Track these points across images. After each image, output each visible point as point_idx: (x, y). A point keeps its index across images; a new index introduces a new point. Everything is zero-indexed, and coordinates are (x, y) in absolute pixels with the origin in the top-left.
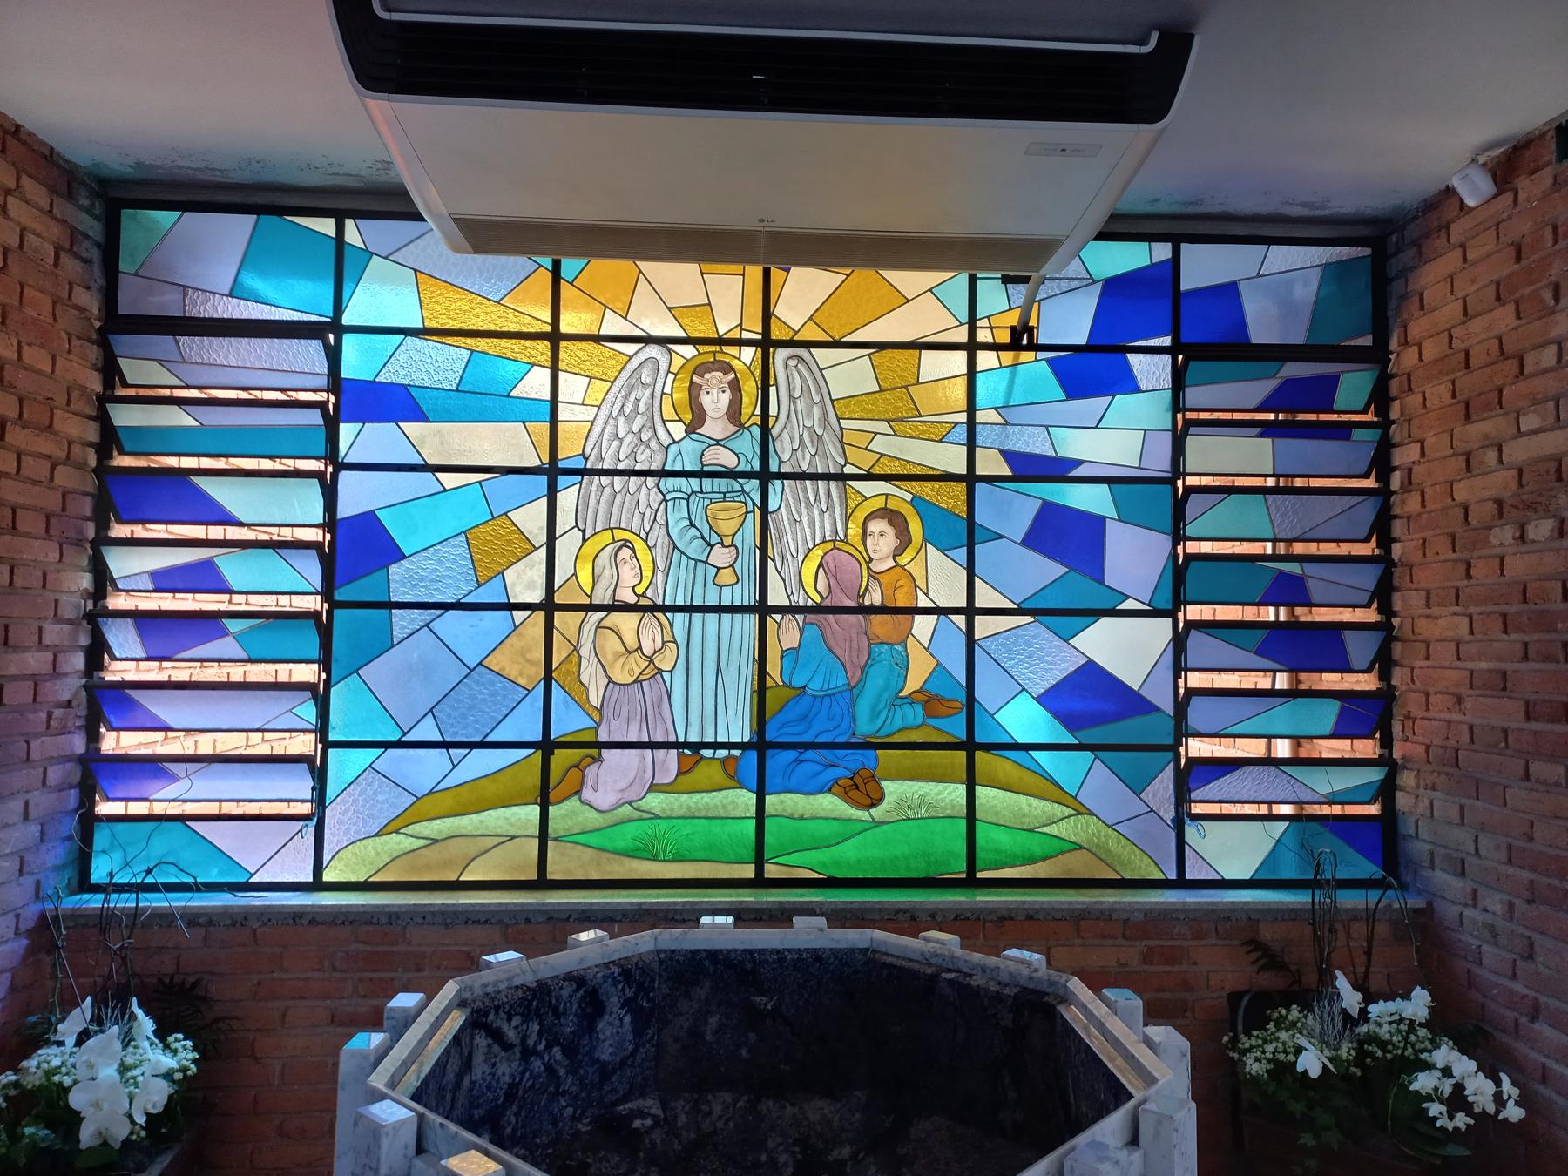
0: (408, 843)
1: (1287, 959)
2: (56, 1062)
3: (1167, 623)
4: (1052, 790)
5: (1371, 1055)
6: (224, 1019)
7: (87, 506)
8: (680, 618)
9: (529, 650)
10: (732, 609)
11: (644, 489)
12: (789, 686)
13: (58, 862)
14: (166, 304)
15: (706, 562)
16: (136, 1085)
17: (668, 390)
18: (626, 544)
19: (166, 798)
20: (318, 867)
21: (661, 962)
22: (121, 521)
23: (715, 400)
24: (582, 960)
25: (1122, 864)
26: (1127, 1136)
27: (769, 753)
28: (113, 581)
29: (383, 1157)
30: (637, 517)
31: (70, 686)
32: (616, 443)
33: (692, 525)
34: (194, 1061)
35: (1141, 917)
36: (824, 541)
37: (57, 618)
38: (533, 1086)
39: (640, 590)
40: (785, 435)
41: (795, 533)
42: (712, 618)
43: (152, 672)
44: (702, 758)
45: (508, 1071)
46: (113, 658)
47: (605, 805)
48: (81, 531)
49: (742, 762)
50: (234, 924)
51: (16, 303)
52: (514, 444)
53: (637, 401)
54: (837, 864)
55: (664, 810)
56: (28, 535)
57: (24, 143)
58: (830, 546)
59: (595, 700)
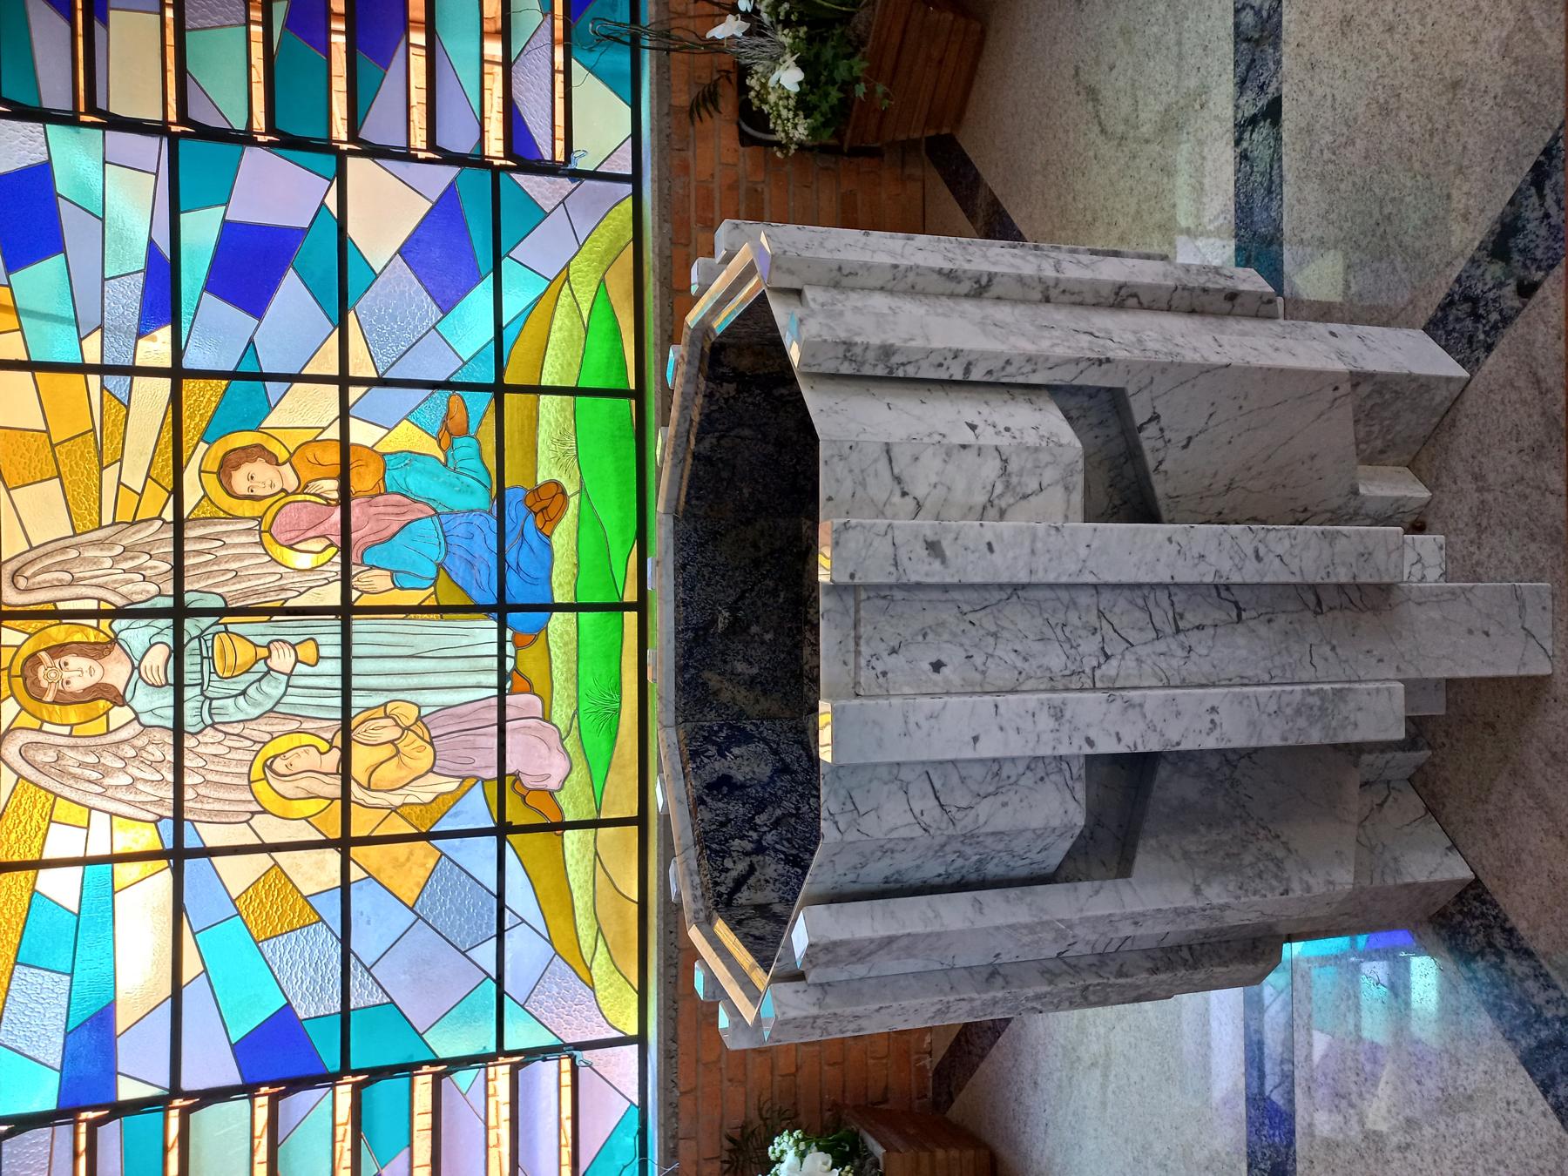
0: (602, 956)
1: (707, 81)
3: (353, 163)
4: (542, 306)
5: (788, 14)
6: (760, 1110)
8: (358, 701)
9: (396, 859)
10: (346, 644)
11: (198, 750)
12: (436, 580)
15: (290, 675)
17: (66, 730)
18: (268, 766)
20: (624, 1041)
21: (686, 721)
23: (79, 673)
24: (680, 802)
25: (618, 239)
26: (794, 300)
27: (509, 600)
29: (804, 1014)
30: (233, 755)
32: (140, 786)
33: (244, 693)
35: (667, 226)
36: (261, 543)
38: (788, 840)
39: (324, 746)
40: (124, 589)
41: (249, 577)
42: (356, 666)
44: (515, 669)
45: (773, 867)
47: (566, 765)
49: (520, 628)
50: (676, 1115)
52: (145, 896)
53: (81, 765)
54: (623, 530)
55: (570, 706)
58: (266, 537)
59: (453, 785)
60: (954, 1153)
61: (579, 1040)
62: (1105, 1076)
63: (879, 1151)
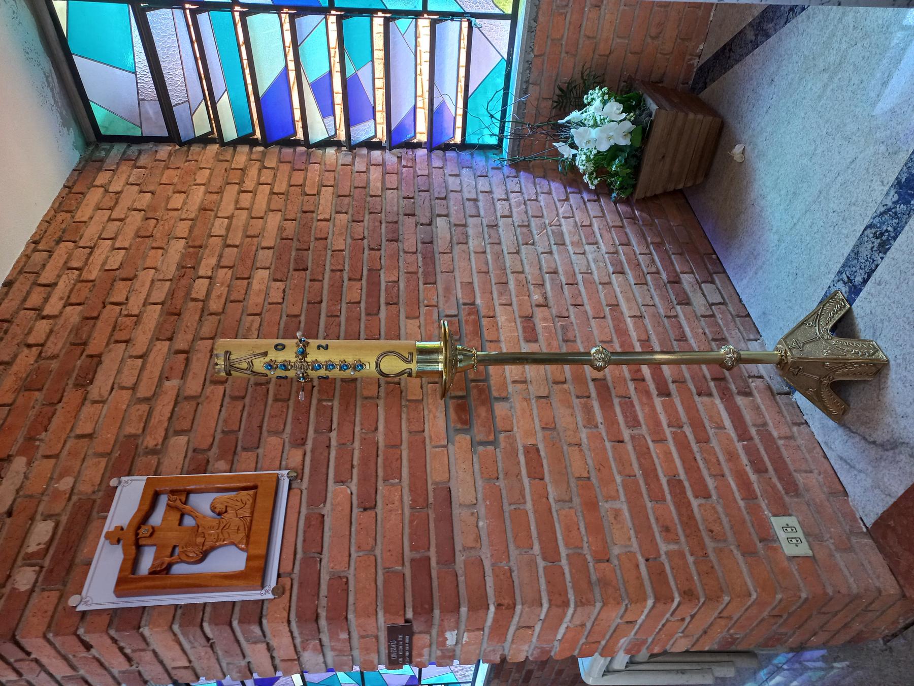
2: (584, 157)
6: (582, 73)
7: (287, 151)
13: (484, 159)
14: (153, 110)
16: (604, 119)
19: (453, 105)
20: (503, 17)
22: (295, 133)
28: (330, 137)
31: (390, 158)
34: (601, 89)
37: (353, 164)
43: (381, 117)
46: (375, 136)
48: (302, 154)
51: (172, 187)
56: (305, 180)
57: (75, 183)
60: (700, 117)
61: (474, 11)
62: (831, 78)
63: (653, 107)
